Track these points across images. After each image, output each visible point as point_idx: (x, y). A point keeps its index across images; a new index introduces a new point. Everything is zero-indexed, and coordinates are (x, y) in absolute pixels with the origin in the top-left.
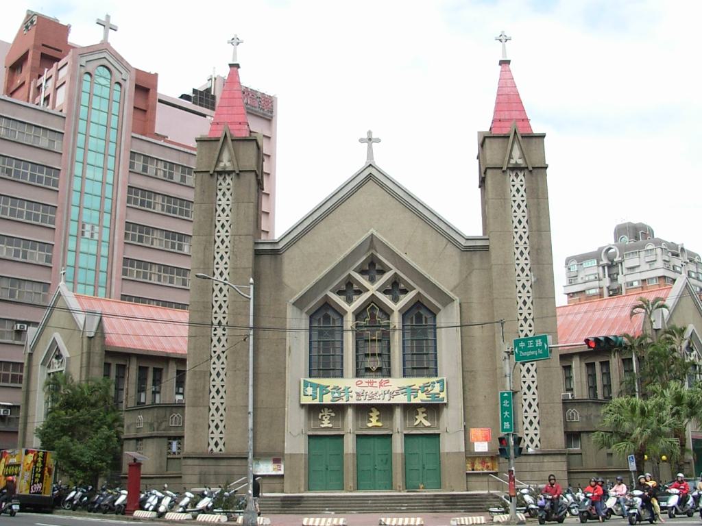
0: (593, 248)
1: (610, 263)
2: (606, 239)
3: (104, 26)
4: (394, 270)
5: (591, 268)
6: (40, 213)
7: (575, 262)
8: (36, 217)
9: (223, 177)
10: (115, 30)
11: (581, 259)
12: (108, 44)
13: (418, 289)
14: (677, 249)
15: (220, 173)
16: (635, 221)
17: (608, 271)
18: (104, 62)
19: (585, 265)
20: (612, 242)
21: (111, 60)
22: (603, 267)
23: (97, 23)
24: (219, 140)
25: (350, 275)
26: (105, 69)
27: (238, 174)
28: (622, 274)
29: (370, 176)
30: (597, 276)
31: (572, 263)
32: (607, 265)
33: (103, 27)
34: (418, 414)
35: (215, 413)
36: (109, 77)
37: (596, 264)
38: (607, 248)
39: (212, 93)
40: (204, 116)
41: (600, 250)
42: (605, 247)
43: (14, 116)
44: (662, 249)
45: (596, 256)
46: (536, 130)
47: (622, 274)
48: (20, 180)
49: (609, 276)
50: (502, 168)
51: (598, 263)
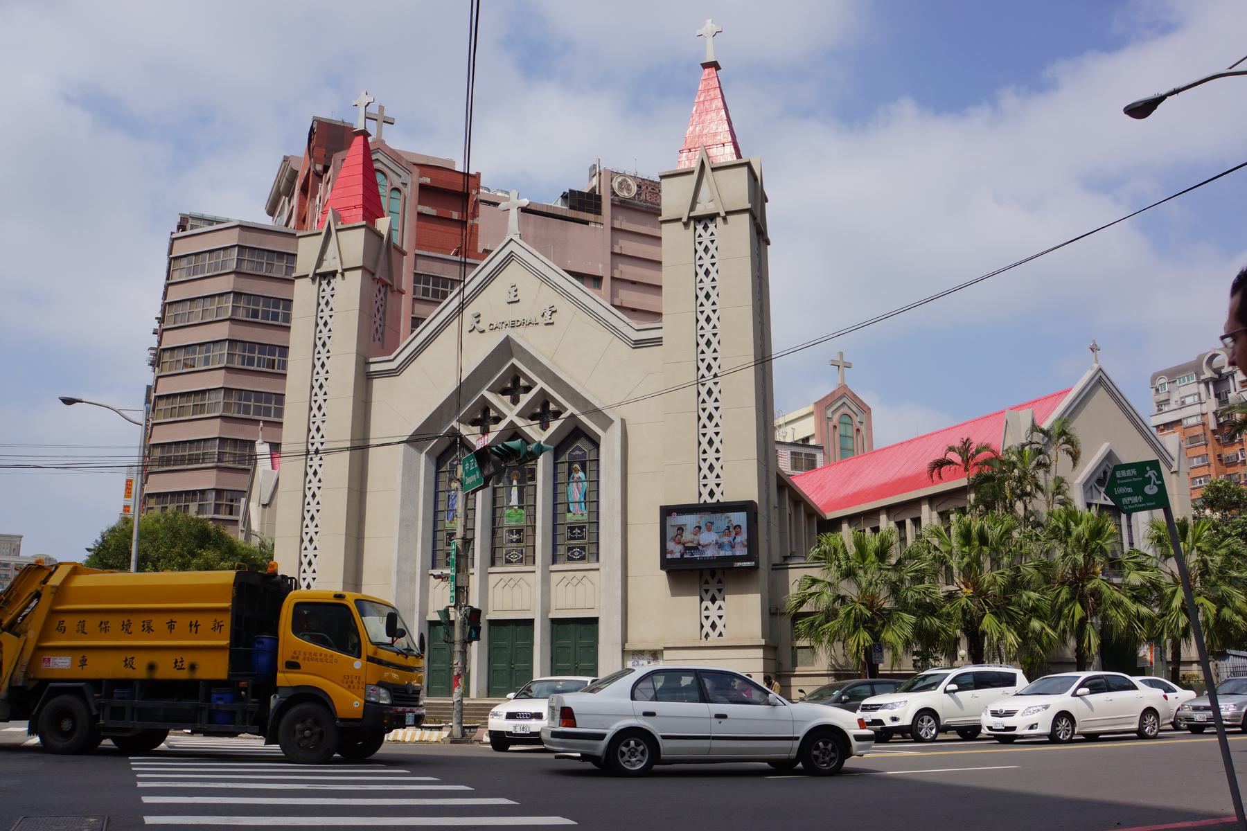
0: (1191, 357)
1: (1217, 376)
3: (376, 120)
6: (280, 311)
8: (255, 314)
10: (393, 124)
11: (1174, 375)
12: (383, 142)
15: (698, 219)
21: (386, 161)
27: (725, 219)
30: (1196, 397)
32: (1212, 379)
33: (375, 121)
35: (705, 324)
37: (1195, 380)
38: (1210, 354)
39: (597, 193)
40: (586, 223)
41: (1201, 357)
42: (1207, 353)
43: (260, 245)
45: (1195, 368)
51: (1198, 377)
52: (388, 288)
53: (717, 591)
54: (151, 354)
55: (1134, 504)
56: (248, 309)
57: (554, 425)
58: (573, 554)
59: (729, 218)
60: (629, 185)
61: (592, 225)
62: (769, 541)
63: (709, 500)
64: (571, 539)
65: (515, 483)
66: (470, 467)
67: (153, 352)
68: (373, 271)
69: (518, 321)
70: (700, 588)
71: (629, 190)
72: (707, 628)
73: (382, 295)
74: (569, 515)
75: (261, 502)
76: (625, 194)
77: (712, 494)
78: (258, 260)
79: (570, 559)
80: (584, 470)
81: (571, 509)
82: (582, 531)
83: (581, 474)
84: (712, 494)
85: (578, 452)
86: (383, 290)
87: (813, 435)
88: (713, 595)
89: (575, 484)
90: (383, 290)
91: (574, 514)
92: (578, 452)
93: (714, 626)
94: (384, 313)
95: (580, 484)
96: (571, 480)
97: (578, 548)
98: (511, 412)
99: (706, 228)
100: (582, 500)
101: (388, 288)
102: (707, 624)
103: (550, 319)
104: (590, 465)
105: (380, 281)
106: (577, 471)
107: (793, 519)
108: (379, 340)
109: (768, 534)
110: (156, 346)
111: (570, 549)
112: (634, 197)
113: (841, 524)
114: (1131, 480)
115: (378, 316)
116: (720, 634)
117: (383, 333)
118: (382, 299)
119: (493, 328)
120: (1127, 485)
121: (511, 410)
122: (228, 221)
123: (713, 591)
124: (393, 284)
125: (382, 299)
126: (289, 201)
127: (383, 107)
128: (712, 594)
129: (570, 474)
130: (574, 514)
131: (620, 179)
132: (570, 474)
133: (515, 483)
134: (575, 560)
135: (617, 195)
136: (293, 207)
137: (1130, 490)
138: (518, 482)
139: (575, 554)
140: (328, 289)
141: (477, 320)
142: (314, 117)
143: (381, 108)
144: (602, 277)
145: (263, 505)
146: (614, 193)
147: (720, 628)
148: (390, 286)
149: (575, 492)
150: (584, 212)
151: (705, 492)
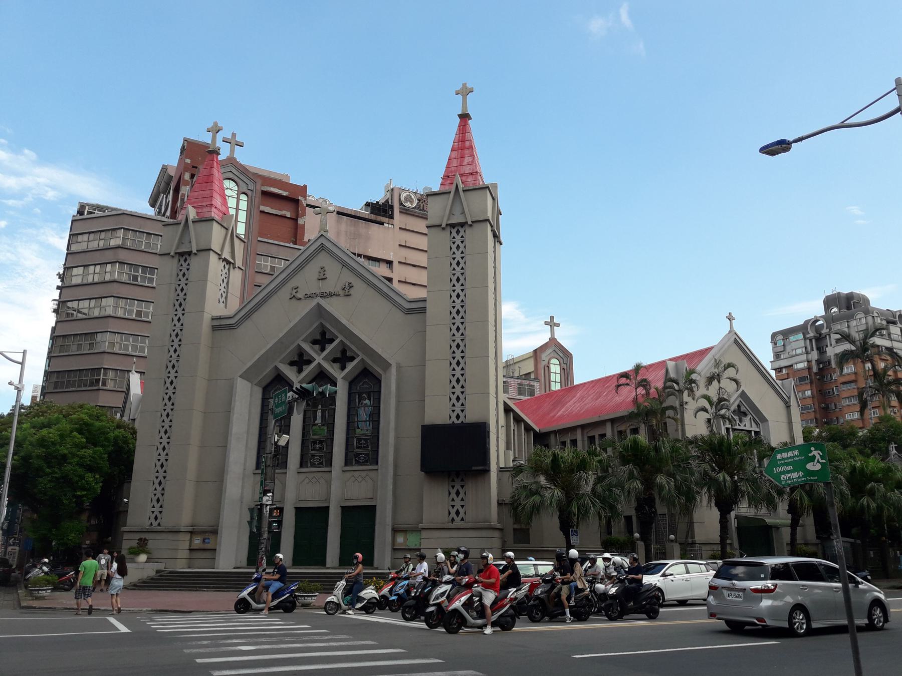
1: (818, 335)
2: (816, 309)
3: (230, 143)
4: (340, 338)
5: (797, 342)
7: (781, 337)
8: (135, 278)
9: (184, 258)
10: (242, 146)
11: (787, 333)
12: (235, 159)
13: (361, 356)
14: (894, 317)
15: (453, 226)
16: (845, 291)
17: (816, 345)
18: (230, 175)
19: (792, 338)
20: (822, 312)
22: (811, 340)
23: (223, 141)
24: (180, 223)
25: (299, 345)
26: (231, 181)
28: (831, 345)
29: (322, 247)
31: (778, 338)
34: (458, 477)
36: (236, 188)
38: (813, 320)
39: (390, 204)
40: (382, 224)
41: (807, 322)
43: (140, 228)
44: (873, 317)
45: (802, 329)
46: (487, 180)
47: (831, 345)
48: (147, 284)
49: (818, 349)
50: (441, 225)
52: (231, 265)
53: (460, 487)
54: (54, 304)
55: (793, 479)
56: (130, 275)
57: (350, 366)
58: (359, 458)
59: (475, 225)
60: (412, 199)
61: (386, 225)
62: (498, 451)
63: (456, 422)
64: (359, 447)
65: (320, 407)
66: (278, 401)
67: (57, 302)
68: (220, 253)
69: (326, 293)
70: (449, 484)
71: (412, 202)
72: (453, 514)
73: (226, 270)
74: (358, 431)
75: (131, 418)
76: (408, 204)
77: (458, 417)
78: (138, 240)
79: (357, 462)
80: (369, 399)
81: (360, 426)
82: (367, 442)
83: (367, 401)
84: (458, 417)
85: (365, 386)
86: (227, 267)
87: (533, 372)
88: (458, 490)
89: (363, 408)
90: (227, 267)
91: (361, 430)
92: (365, 386)
93: (458, 513)
94: (228, 283)
95: (367, 409)
96: (360, 405)
97: (363, 454)
98: (320, 359)
99: (458, 232)
100: (368, 419)
101: (231, 265)
102: (453, 511)
103: (348, 292)
104: (375, 396)
105: (225, 260)
106: (364, 399)
107: (516, 433)
108: (223, 302)
109: (498, 445)
110: (58, 298)
111: (358, 455)
112: (415, 207)
113: (550, 436)
114: (793, 460)
115: (223, 286)
116: (462, 519)
117: (226, 298)
118: (226, 273)
119: (309, 297)
120: (787, 464)
121: (319, 355)
122: (120, 210)
123: (458, 487)
124: (235, 263)
125: (226, 273)
126: (166, 198)
127: (236, 134)
128: (456, 489)
129: (360, 401)
130: (361, 430)
131: (405, 194)
132: (360, 401)
133: (320, 407)
134: (361, 463)
135: (404, 206)
136: (169, 202)
137: (790, 468)
138: (322, 407)
139: (363, 458)
140: (185, 265)
141: (296, 290)
142: (184, 138)
143: (234, 135)
144: (393, 261)
145: (132, 419)
146: (401, 204)
147: (462, 515)
148: (233, 264)
149: (363, 414)
150: (381, 216)
151: (454, 415)
